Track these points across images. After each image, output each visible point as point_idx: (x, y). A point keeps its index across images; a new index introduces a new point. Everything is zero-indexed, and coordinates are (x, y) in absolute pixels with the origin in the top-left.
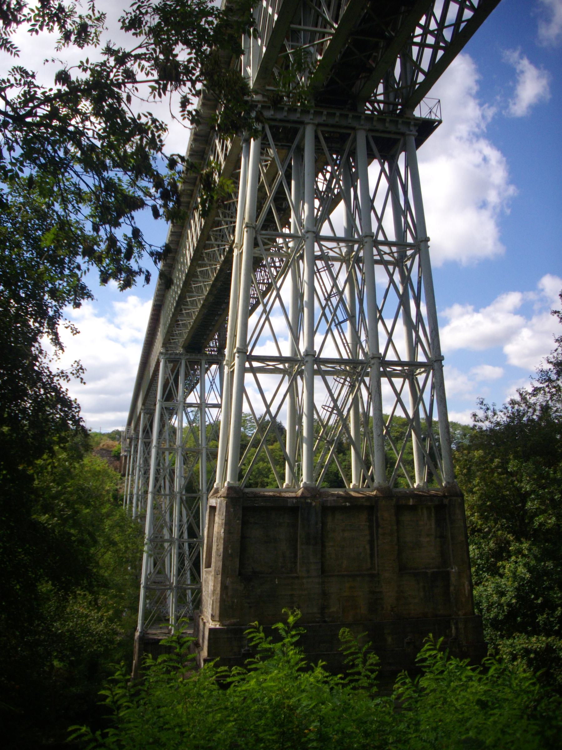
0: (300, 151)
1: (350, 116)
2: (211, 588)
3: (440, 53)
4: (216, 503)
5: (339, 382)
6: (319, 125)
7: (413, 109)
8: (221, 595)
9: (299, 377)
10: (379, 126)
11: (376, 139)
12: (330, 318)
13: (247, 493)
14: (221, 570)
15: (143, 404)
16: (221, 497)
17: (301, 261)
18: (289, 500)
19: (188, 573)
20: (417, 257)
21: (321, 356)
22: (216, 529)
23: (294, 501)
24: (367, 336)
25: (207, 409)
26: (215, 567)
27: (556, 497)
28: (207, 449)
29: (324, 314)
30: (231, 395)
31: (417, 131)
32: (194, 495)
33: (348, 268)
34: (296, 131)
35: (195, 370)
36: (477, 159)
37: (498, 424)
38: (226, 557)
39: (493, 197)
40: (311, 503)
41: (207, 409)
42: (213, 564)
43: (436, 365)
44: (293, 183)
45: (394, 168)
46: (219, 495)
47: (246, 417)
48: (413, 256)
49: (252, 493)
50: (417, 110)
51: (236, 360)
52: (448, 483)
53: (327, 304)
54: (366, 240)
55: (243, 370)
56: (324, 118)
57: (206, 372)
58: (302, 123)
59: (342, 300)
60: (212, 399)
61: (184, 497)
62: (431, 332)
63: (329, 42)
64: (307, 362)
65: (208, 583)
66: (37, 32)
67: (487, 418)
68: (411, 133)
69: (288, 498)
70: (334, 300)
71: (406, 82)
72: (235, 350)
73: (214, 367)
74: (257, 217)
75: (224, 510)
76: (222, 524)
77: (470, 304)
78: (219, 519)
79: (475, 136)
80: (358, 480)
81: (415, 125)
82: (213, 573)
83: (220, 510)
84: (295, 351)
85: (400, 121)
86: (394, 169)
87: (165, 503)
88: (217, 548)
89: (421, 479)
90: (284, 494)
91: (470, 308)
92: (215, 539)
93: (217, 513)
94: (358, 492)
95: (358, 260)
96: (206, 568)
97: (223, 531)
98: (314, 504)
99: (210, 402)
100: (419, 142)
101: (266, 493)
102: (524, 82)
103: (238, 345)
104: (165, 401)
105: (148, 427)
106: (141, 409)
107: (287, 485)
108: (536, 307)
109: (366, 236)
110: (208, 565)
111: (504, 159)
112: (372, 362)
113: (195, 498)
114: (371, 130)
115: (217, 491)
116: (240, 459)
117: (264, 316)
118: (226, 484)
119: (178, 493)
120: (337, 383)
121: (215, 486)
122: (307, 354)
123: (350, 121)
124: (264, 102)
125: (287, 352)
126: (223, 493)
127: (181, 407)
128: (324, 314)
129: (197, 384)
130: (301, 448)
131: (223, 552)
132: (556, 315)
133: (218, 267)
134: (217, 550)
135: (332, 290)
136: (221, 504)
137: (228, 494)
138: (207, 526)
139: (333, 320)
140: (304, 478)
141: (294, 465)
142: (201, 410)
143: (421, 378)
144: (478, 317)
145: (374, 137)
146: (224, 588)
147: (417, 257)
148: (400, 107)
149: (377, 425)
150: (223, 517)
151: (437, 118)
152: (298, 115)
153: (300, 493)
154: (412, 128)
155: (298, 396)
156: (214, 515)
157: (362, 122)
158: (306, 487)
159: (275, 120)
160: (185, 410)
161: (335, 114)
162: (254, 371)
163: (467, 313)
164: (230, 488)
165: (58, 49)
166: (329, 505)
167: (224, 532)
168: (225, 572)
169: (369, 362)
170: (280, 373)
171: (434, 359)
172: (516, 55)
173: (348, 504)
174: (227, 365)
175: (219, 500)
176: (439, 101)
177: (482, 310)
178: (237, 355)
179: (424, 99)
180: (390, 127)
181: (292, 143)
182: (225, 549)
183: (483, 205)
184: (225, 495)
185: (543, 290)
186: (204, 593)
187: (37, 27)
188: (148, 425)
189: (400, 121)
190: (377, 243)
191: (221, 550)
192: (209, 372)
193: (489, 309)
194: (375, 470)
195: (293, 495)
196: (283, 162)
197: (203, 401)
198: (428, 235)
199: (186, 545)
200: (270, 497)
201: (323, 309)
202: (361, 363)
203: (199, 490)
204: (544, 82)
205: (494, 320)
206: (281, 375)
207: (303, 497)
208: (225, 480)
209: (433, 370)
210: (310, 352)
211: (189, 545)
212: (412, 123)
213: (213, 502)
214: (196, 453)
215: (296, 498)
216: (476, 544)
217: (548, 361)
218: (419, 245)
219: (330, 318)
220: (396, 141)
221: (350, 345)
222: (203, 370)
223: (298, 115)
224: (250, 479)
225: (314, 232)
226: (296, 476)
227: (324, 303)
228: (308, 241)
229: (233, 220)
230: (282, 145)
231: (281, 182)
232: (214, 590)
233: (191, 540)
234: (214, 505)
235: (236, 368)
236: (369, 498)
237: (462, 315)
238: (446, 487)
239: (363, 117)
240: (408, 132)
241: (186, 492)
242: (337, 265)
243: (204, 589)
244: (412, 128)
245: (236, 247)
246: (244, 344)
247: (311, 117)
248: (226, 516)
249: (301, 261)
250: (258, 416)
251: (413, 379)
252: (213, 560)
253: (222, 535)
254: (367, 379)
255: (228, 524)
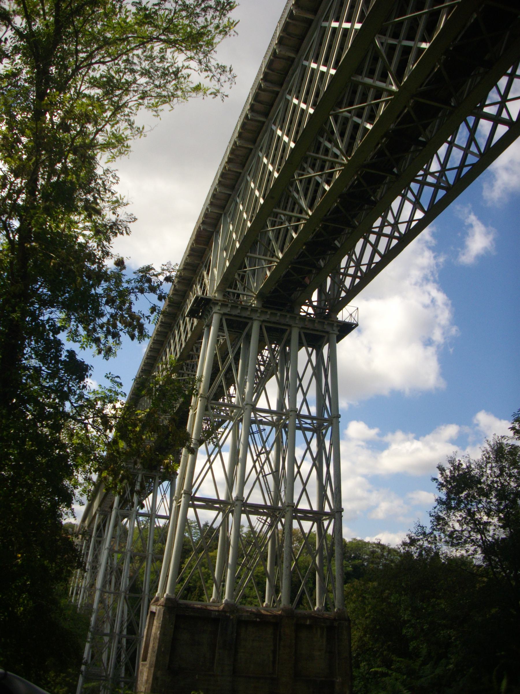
0: (248, 337)
1: (288, 316)
2: (145, 677)
3: (357, 281)
4: (156, 610)
5: (261, 522)
6: (264, 321)
7: (337, 314)
8: (152, 685)
9: (230, 515)
10: (310, 326)
11: (306, 335)
12: (259, 469)
13: (181, 604)
14: (154, 664)
15: (100, 506)
16: (160, 605)
17: (241, 423)
18: (213, 613)
19: (123, 668)
20: (330, 429)
21: (248, 502)
22: (154, 630)
23: (217, 613)
24: (285, 488)
25: (156, 519)
26: (150, 662)
27: (425, 627)
28: (153, 555)
29: (254, 466)
30: (176, 525)
31: (339, 331)
32: (137, 595)
33: (276, 432)
34: (247, 324)
35: (150, 483)
36: (427, 300)
37: (392, 561)
38: (160, 654)
39: (438, 336)
40: (229, 617)
41: (156, 519)
42: (148, 659)
43: (337, 515)
44: (240, 361)
45: (319, 355)
46: (159, 603)
47: (192, 523)
48: (327, 428)
49: (185, 604)
50: (340, 313)
51: (183, 499)
52: (339, 609)
53: (257, 460)
54: (291, 413)
55: (187, 506)
56: (268, 316)
57: (159, 486)
58: (251, 319)
59: (268, 458)
60: (163, 511)
61: (127, 596)
62: (336, 489)
63: (274, 267)
64: (237, 505)
65: (143, 674)
66: (84, 349)
67: (382, 555)
68: (335, 332)
69: (212, 610)
70: (263, 457)
71: (334, 292)
72: (182, 492)
73: (166, 483)
74: (210, 388)
75: (161, 616)
76: (159, 627)
77: (412, 433)
78: (156, 623)
79: (426, 279)
80: (270, 600)
81: (337, 326)
82: (148, 666)
83: (158, 616)
84: (229, 497)
85: (326, 322)
86: (319, 356)
87: (110, 600)
88: (153, 645)
89: (320, 603)
90: (209, 608)
91: (411, 436)
92: (152, 639)
93: (156, 618)
94: (267, 611)
95: (285, 426)
96: (143, 661)
97: (159, 632)
98: (232, 617)
99: (159, 514)
100: (340, 338)
101: (195, 606)
102: (473, 236)
103: (185, 488)
104: (120, 509)
105: (102, 526)
106: (97, 510)
107: (214, 599)
108: (470, 439)
109: (291, 411)
110: (145, 659)
111: (450, 302)
112: (287, 509)
113: (139, 598)
114: (303, 328)
115: (158, 600)
116: (179, 575)
117: (208, 465)
118: (165, 596)
119: (123, 592)
120: (259, 522)
121: (157, 595)
122: (237, 499)
123: (287, 320)
124: (224, 301)
125: (222, 497)
126: (163, 602)
127: (134, 515)
128: (254, 466)
129: (149, 494)
130: (226, 571)
131: (158, 649)
132: (435, 481)
133: (178, 405)
134: (153, 647)
135: (262, 450)
136: (159, 611)
137: (165, 604)
138: (147, 627)
139: (261, 471)
140: (226, 596)
141: (220, 584)
142: (151, 520)
143: (326, 523)
144: (417, 444)
145: (304, 333)
146: (155, 678)
147: (330, 429)
148: (327, 311)
149: (286, 559)
150: (160, 622)
151: (355, 322)
152: (249, 313)
153: (221, 607)
154: (335, 328)
155: (228, 530)
156: (154, 619)
157: (297, 322)
158: (227, 604)
159: (230, 315)
160: (137, 518)
161: (276, 314)
162: (195, 507)
163: (408, 440)
164: (168, 599)
165: (94, 356)
166: (243, 619)
167: (160, 634)
168: (157, 666)
169: (285, 509)
170: (216, 510)
171: (336, 511)
172: (466, 211)
173: (258, 620)
174: (176, 500)
175: (158, 608)
176: (358, 309)
177: (421, 438)
178: (183, 495)
179: (346, 307)
180: (318, 326)
181: (243, 331)
182: (159, 647)
183: (428, 342)
184: (164, 604)
185: (477, 425)
186: (139, 682)
187: (84, 346)
188: (102, 525)
189: (326, 322)
190: (300, 416)
191: (156, 648)
192: (161, 486)
193: (428, 438)
194: (284, 595)
195: (216, 608)
196: (233, 346)
197: (154, 512)
198: (340, 413)
199: (124, 641)
200: (198, 608)
201: (254, 462)
202: (279, 509)
203: (142, 591)
204: (491, 237)
205: (432, 448)
206: (217, 512)
207: (223, 611)
208: (165, 592)
209: (335, 519)
210: (240, 498)
211: (127, 641)
212: (335, 325)
213: (153, 608)
214: (143, 559)
215: (218, 611)
216: (366, 661)
217: (430, 514)
218: (332, 420)
219: (259, 469)
220: (323, 337)
221: (272, 493)
222: (157, 483)
223: (249, 313)
224: (189, 583)
225: (252, 405)
226: (220, 594)
227: (255, 458)
228: (247, 412)
229: (193, 373)
230: (235, 331)
231: (231, 364)
232: (147, 680)
233: (130, 636)
234: (154, 611)
235: (182, 504)
236: (275, 616)
237: (404, 441)
238: (337, 612)
239: (298, 318)
240: (331, 332)
241: (129, 592)
242: (268, 428)
243: (139, 679)
244: (335, 328)
245: (192, 409)
246: (191, 486)
247: (259, 315)
248: (163, 621)
249: (241, 423)
250: (202, 523)
251: (320, 523)
252: (149, 655)
253: (158, 636)
254: (283, 520)
255: (163, 628)
